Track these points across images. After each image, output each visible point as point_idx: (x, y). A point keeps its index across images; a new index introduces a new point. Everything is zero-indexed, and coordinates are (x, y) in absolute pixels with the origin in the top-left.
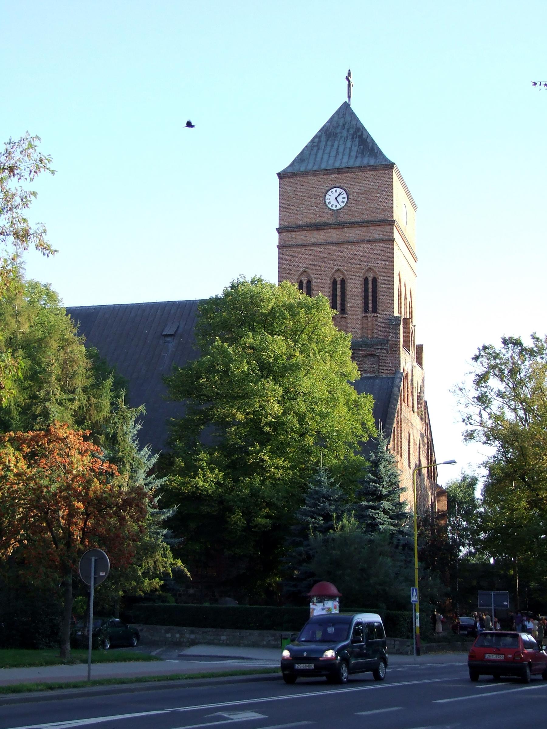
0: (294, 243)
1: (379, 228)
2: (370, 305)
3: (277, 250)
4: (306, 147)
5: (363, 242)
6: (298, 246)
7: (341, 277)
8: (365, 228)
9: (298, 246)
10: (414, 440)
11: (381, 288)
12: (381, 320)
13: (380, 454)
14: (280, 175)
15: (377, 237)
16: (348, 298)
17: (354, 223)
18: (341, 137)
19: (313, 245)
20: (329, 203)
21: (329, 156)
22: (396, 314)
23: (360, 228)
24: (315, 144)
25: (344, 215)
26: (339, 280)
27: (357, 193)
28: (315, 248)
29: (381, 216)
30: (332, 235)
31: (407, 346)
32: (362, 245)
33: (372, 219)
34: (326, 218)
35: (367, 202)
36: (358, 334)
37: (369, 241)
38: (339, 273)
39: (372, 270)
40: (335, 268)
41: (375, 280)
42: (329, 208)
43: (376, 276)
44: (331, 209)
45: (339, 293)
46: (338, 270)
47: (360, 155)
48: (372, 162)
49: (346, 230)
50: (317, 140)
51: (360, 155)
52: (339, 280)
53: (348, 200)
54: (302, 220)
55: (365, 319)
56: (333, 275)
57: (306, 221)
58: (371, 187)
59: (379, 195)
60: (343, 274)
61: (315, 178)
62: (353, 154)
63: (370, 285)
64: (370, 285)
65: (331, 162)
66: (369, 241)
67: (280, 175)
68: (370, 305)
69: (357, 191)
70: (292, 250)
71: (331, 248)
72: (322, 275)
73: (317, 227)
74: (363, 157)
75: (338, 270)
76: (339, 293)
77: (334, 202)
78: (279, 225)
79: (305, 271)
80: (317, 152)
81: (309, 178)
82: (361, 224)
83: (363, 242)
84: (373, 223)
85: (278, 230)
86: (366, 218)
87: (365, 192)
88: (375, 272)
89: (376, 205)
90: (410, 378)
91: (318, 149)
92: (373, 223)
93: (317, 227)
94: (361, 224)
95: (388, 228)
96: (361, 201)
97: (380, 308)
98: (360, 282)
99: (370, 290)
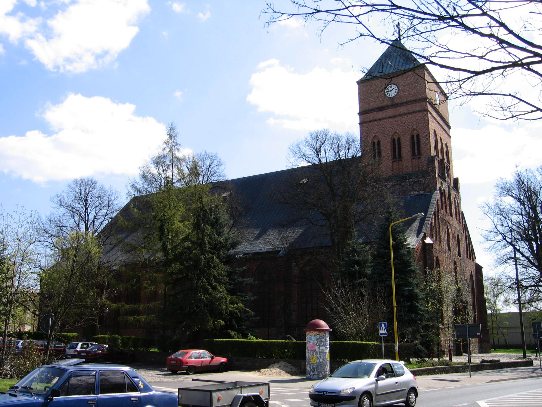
0: (368, 120)
1: (418, 104)
2: (416, 152)
3: (359, 126)
4: (373, 65)
5: (409, 113)
6: (370, 121)
7: (398, 136)
8: (410, 105)
9: (370, 121)
10: (453, 234)
11: (422, 140)
12: (424, 160)
13: (428, 314)
14: (358, 83)
15: (417, 109)
16: (402, 149)
17: (403, 103)
18: (394, 57)
19: (380, 120)
20: (395, 92)
21: (387, 68)
22: (433, 153)
23: (407, 106)
24: (379, 63)
25: (396, 100)
26: (396, 139)
27: (404, 85)
28: (381, 121)
29: (420, 96)
30: (391, 112)
31: (442, 177)
32: (409, 116)
33: (414, 99)
34: (386, 103)
35: (410, 90)
36: (409, 169)
37: (412, 113)
38: (396, 134)
39: (416, 129)
40: (394, 132)
41: (418, 136)
42: (387, 97)
43: (418, 133)
44: (389, 97)
45: (397, 146)
46: (396, 132)
47: (404, 64)
48: (412, 66)
49: (398, 108)
50: (379, 61)
51: (404, 64)
52: (396, 139)
53: (398, 90)
54: (373, 106)
55: (413, 160)
56: (393, 135)
57: (375, 106)
58: (412, 81)
59: (417, 85)
60: (399, 135)
61: (378, 81)
62: (401, 64)
63: (415, 139)
64: (415, 139)
65: (388, 70)
66: (412, 113)
67: (358, 83)
68: (416, 152)
69: (403, 84)
70: (368, 124)
71: (390, 120)
72: (386, 137)
73: (381, 109)
74: (406, 64)
75: (396, 132)
76: (397, 146)
77: (394, 91)
78: (359, 110)
79: (375, 136)
80: (380, 67)
81: (374, 82)
82: (407, 103)
83: (409, 113)
84: (415, 101)
85: (359, 114)
86: (410, 99)
87: (408, 84)
88: (417, 131)
89: (416, 91)
90: (447, 195)
91: (380, 65)
92: (415, 101)
93: (381, 109)
94: (407, 103)
95: (424, 103)
96: (406, 90)
97: (423, 152)
98: (408, 138)
99: (416, 142)
